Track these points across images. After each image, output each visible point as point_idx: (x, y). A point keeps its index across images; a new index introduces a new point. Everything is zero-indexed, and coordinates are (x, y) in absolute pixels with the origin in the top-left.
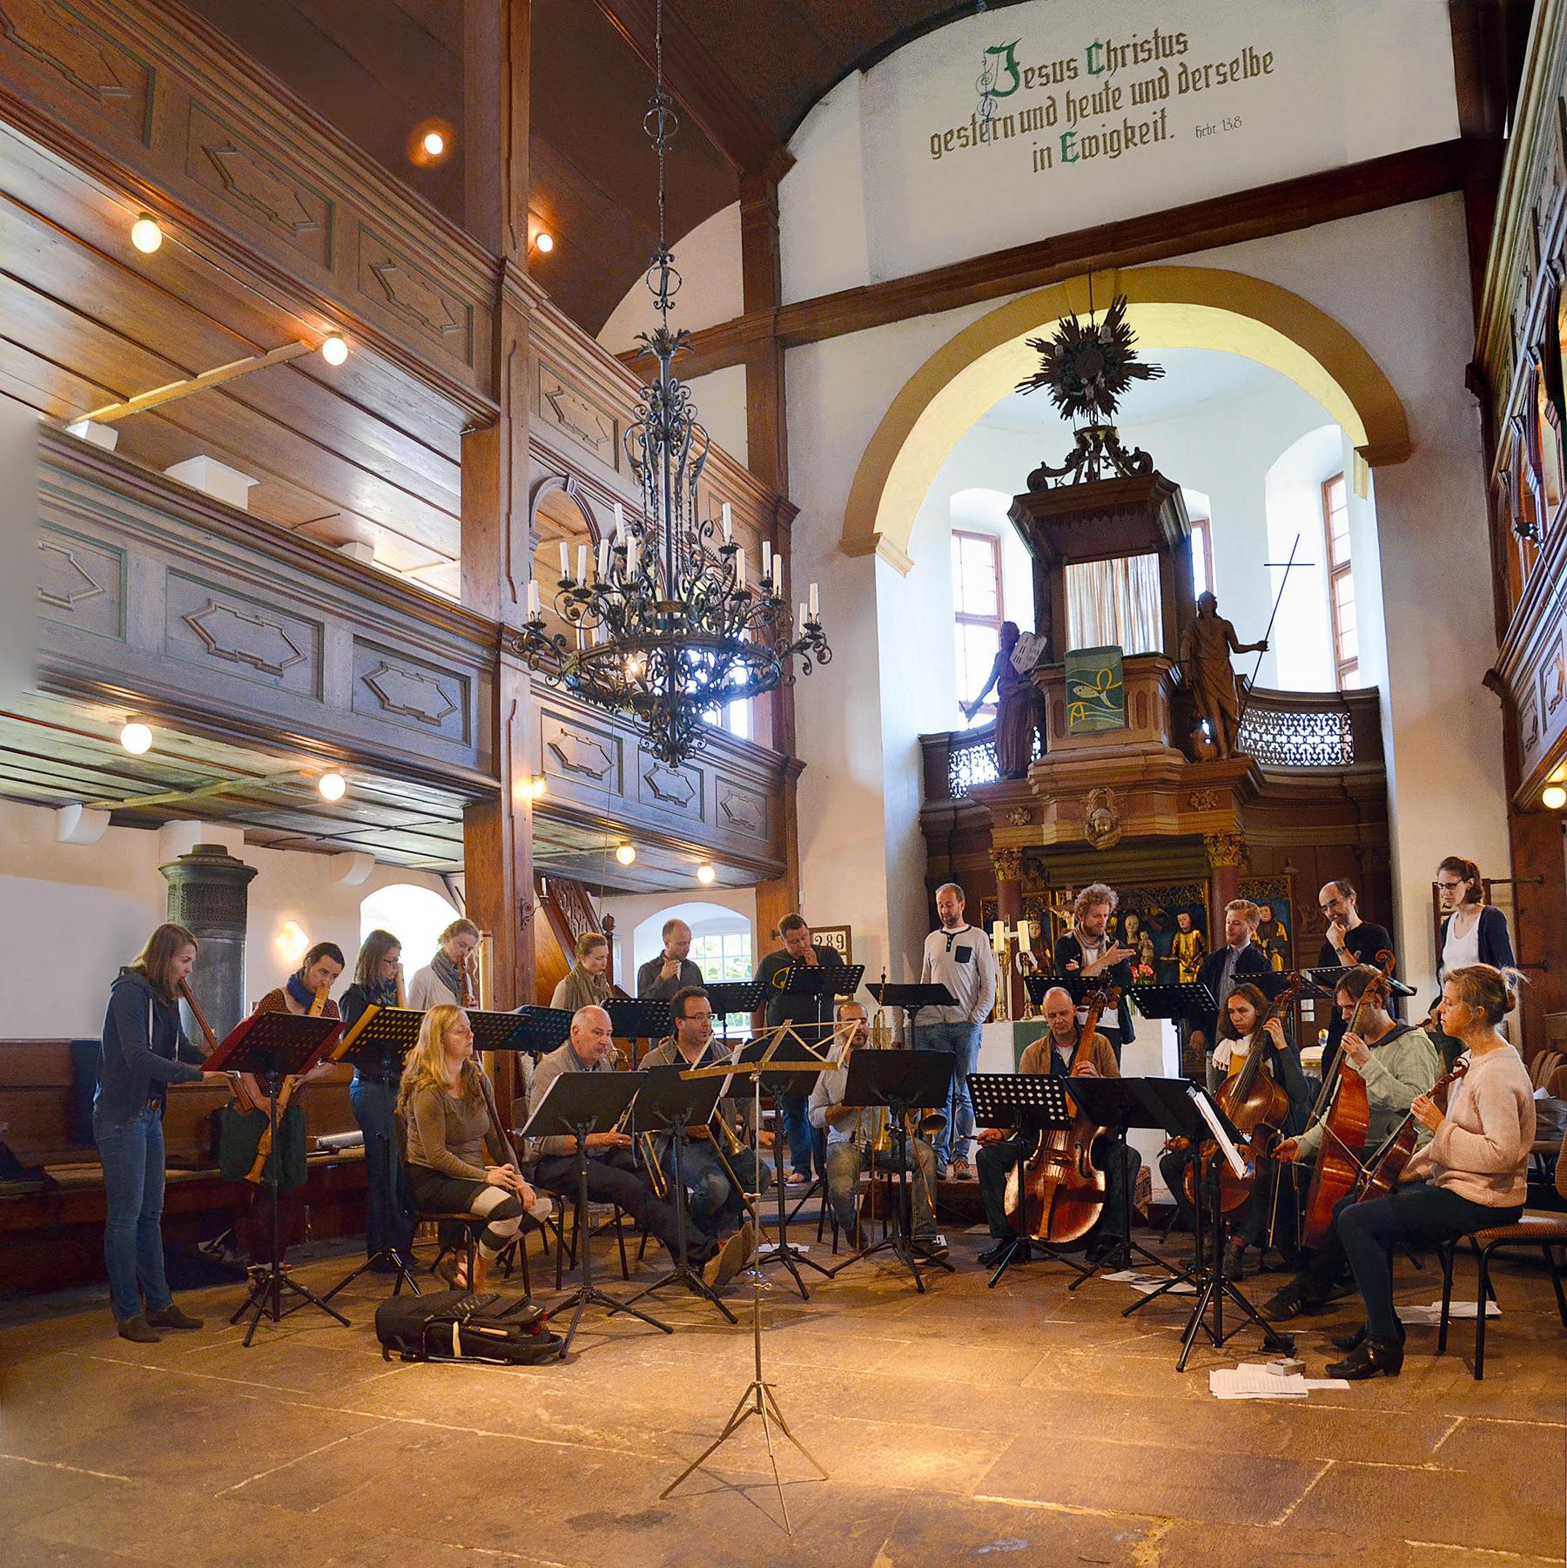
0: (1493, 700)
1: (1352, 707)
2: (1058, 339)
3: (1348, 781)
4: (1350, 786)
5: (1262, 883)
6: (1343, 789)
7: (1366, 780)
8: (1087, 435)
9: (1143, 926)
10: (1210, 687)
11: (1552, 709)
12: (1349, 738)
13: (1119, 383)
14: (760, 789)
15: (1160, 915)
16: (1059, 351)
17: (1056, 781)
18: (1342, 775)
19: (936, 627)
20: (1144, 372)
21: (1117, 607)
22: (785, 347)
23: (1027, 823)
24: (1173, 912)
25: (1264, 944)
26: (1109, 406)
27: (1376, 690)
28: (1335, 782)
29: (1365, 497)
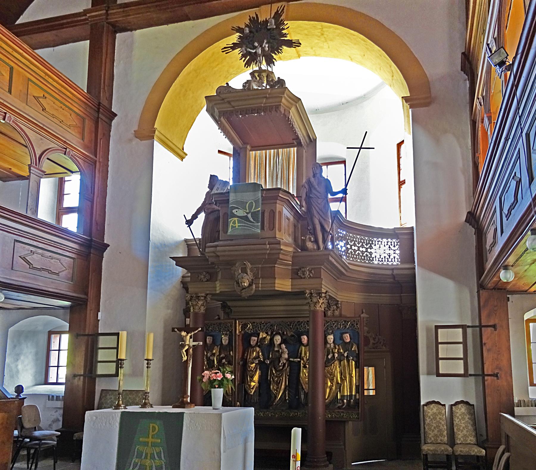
0: (471, 230)
1: (400, 237)
2: (247, 26)
3: (395, 272)
4: (397, 274)
5: (345, 321)
6: (394, 276)
7: (406, 272)
8: (256, 75)
9: (283, 341)
10: (315, 212)
11: (508, 216)
12: (398, 252)
13: (276, 49)
14: (73, 256)
15: (292, 336)
16: (247, 30)
17: (218, 256)
18: (393, 269)
19: (183, 178)
20: (290, 44)
21: (275, 169)
22: (116, 32)
23: (207, 281)
24: (300, 335)
25: (346, 355)
26: (270, 61)
27: (412, 228)
28: (389, 272)
29: (410, 134)
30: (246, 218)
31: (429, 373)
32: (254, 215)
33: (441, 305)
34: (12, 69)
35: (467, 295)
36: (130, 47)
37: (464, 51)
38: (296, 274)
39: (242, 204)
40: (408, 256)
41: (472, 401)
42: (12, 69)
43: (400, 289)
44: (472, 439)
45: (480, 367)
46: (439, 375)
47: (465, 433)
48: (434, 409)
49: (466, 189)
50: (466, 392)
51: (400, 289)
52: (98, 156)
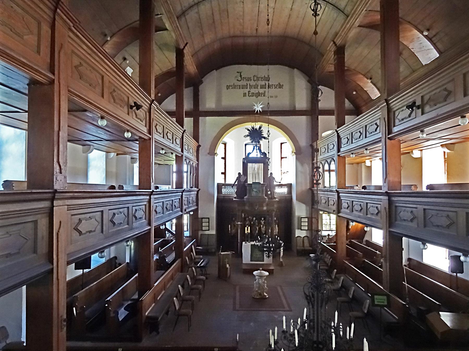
30: (256, 192)
31: (298, 229)
32: (259, 191)
33: (300, 211)
34: (164, 127)
35: (308, 208)
36: (205, 123)
37: (317, 36)
38: (267, 205)
39: (255, 188)
40: (290, 192)
41: (308, 236)
42: (164, 127)
43: (287, 203)
44: (308, 245)
45: (59, 243)
46: (301, 230)
47: (307, 244)
48: (299, 238)
49: (310, 183)
50: (307, 234)
51: (287, 203)
52: (56, 72)
